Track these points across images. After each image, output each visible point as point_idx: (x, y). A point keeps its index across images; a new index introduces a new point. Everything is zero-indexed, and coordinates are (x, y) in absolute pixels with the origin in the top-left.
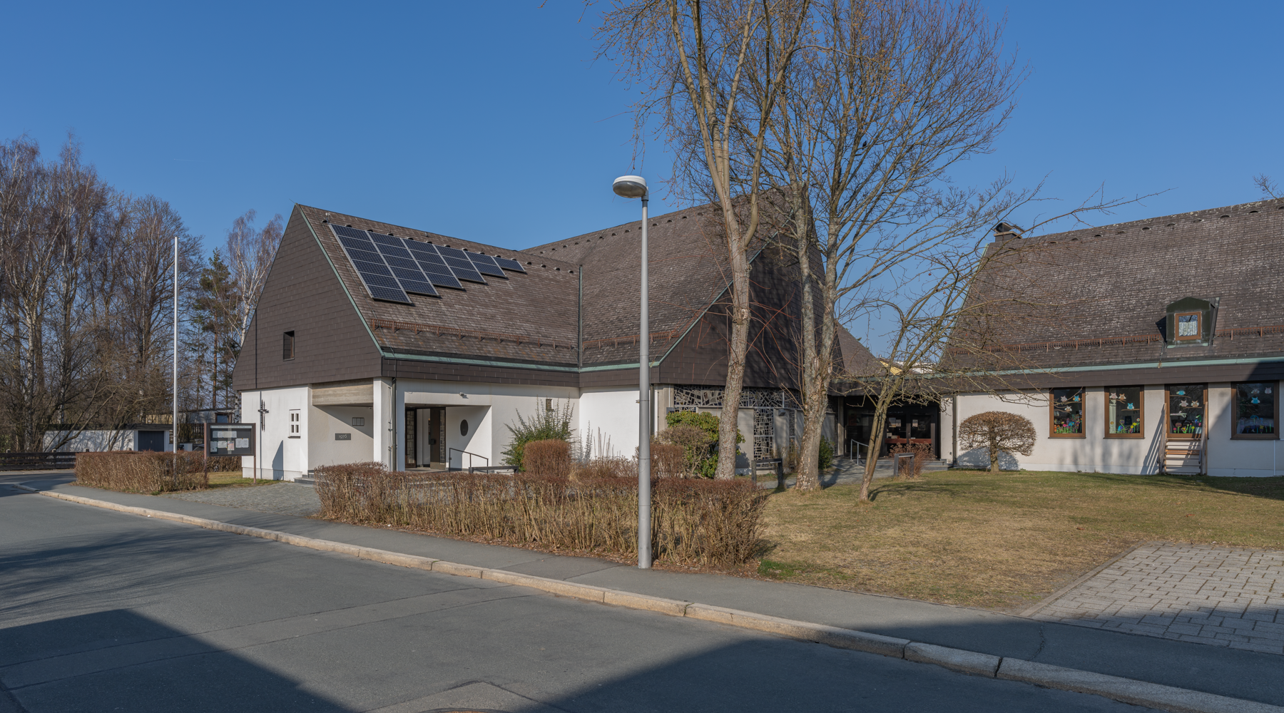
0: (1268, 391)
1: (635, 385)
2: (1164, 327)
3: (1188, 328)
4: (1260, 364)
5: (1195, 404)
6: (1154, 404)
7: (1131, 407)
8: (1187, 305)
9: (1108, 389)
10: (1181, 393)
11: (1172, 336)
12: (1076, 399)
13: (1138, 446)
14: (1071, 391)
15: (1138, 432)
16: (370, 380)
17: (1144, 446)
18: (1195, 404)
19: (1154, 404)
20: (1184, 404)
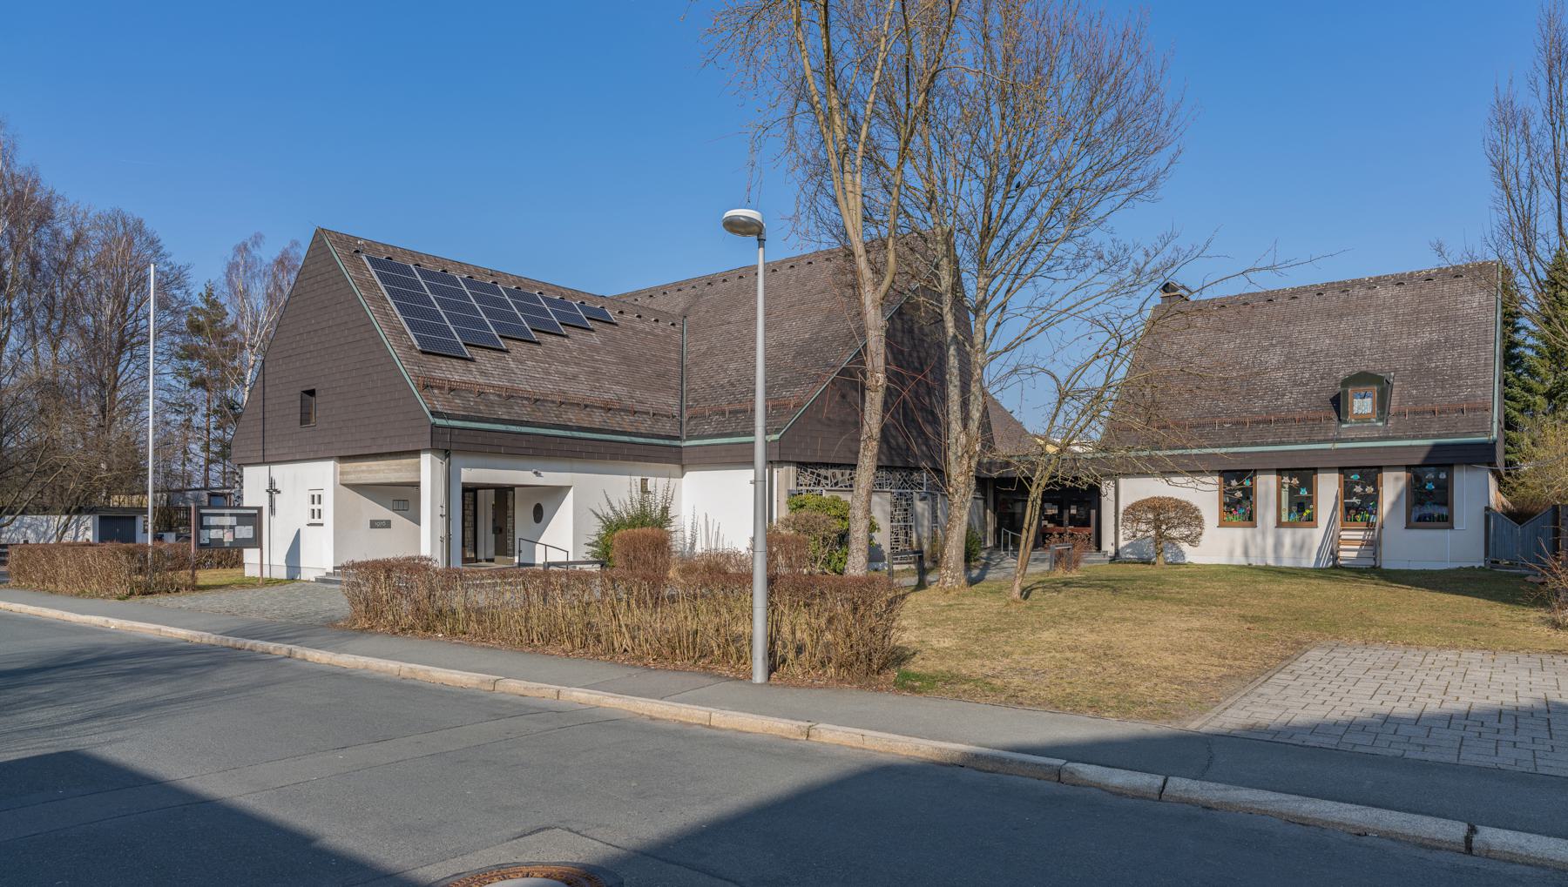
0: (1443, 476)
1: (749, 463)
2: (1338, 404)
3: (1362, 405)
4: (1435, 446)
5: (1370, 490)
6: (1328, 488)
7: (1304, 492)
8: (1362, 379)
9: (1280, 472)
10: (1355, 477)
11: (1346, 413)
12: (1247, 483)
13: (1311, 536)
14: (1241, 474)
15: (1311, 520)
16: (416, 453)
17: (1317, 535)
18: (1370, 490)
19: (1328, 488)
20: (1358, 489)
